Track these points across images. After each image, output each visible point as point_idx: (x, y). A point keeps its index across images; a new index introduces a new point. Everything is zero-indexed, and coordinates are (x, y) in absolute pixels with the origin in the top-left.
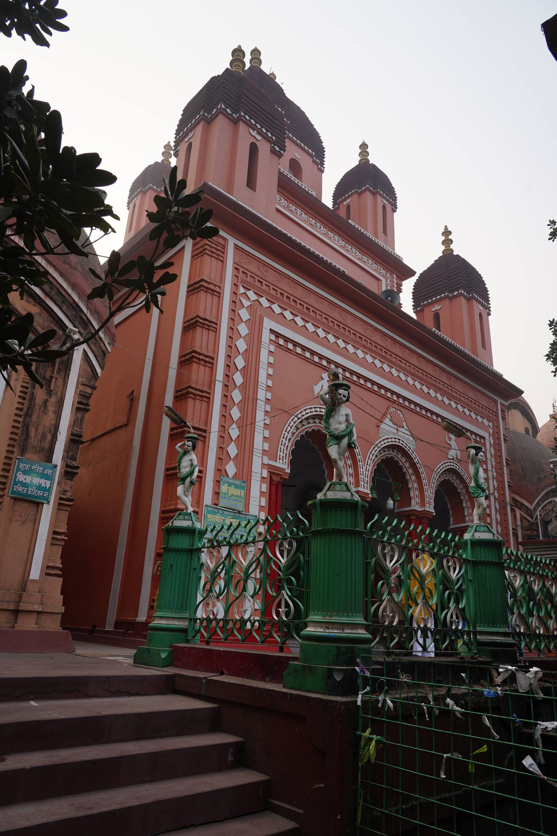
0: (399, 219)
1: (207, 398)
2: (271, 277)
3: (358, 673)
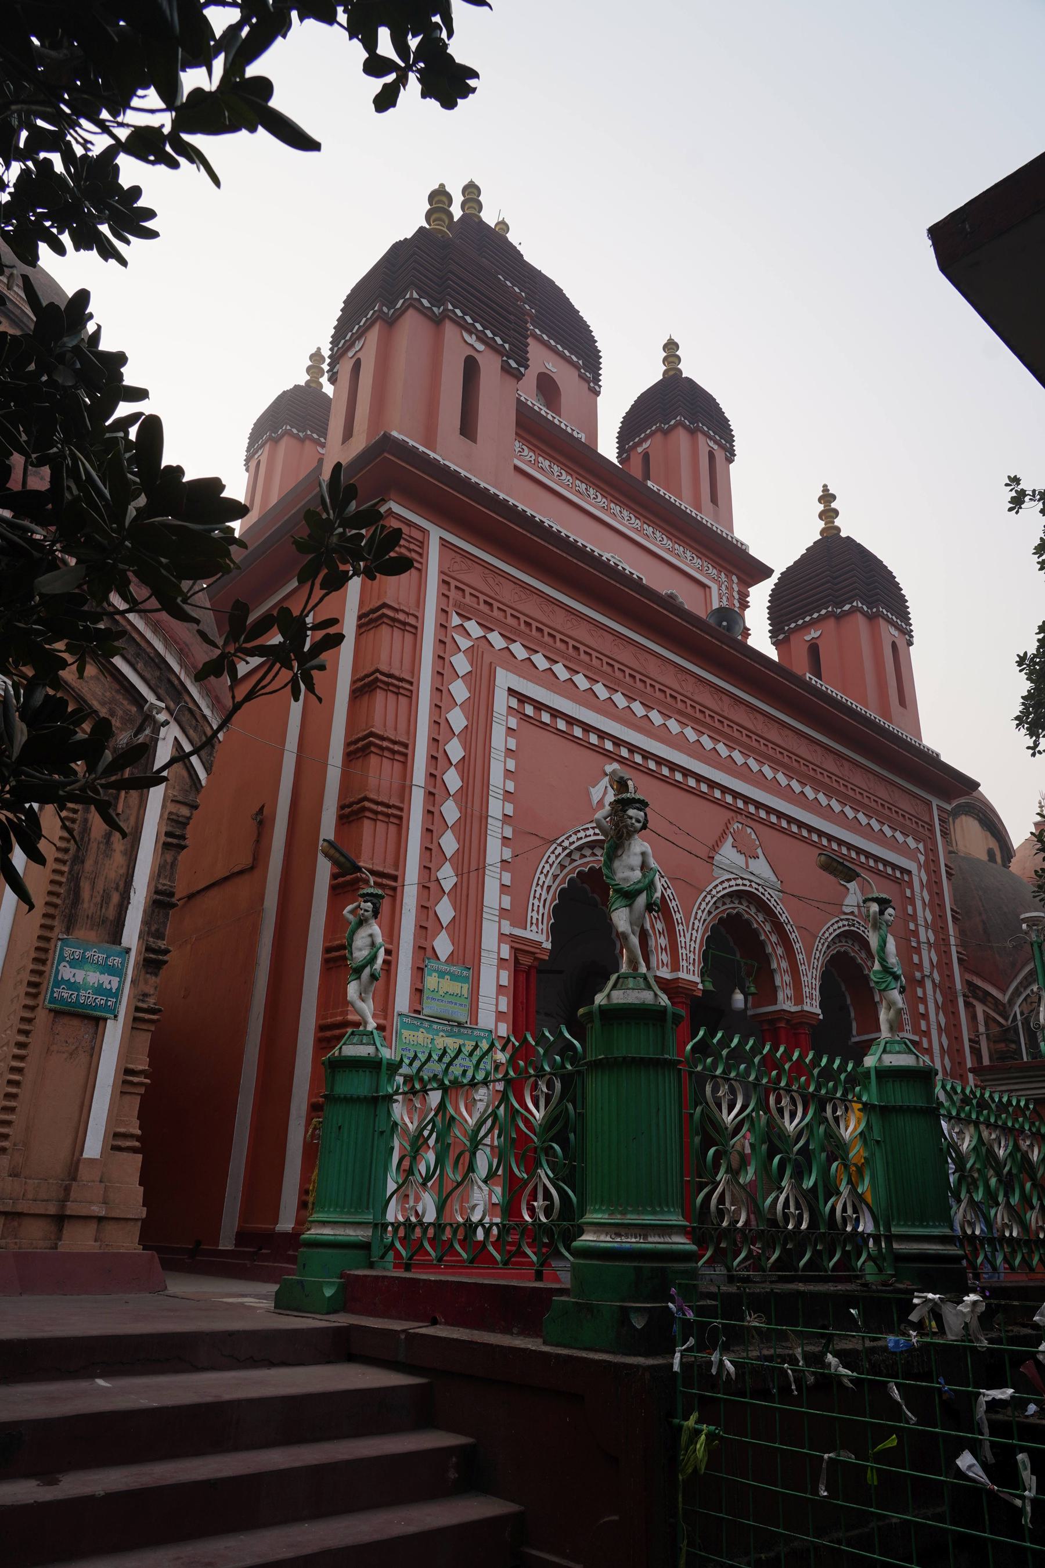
0: (740, 475)
1: (398, 818)
2: (507, 594)
3: (672, 1312)
